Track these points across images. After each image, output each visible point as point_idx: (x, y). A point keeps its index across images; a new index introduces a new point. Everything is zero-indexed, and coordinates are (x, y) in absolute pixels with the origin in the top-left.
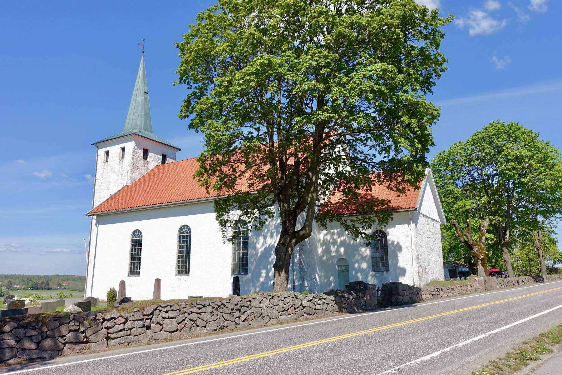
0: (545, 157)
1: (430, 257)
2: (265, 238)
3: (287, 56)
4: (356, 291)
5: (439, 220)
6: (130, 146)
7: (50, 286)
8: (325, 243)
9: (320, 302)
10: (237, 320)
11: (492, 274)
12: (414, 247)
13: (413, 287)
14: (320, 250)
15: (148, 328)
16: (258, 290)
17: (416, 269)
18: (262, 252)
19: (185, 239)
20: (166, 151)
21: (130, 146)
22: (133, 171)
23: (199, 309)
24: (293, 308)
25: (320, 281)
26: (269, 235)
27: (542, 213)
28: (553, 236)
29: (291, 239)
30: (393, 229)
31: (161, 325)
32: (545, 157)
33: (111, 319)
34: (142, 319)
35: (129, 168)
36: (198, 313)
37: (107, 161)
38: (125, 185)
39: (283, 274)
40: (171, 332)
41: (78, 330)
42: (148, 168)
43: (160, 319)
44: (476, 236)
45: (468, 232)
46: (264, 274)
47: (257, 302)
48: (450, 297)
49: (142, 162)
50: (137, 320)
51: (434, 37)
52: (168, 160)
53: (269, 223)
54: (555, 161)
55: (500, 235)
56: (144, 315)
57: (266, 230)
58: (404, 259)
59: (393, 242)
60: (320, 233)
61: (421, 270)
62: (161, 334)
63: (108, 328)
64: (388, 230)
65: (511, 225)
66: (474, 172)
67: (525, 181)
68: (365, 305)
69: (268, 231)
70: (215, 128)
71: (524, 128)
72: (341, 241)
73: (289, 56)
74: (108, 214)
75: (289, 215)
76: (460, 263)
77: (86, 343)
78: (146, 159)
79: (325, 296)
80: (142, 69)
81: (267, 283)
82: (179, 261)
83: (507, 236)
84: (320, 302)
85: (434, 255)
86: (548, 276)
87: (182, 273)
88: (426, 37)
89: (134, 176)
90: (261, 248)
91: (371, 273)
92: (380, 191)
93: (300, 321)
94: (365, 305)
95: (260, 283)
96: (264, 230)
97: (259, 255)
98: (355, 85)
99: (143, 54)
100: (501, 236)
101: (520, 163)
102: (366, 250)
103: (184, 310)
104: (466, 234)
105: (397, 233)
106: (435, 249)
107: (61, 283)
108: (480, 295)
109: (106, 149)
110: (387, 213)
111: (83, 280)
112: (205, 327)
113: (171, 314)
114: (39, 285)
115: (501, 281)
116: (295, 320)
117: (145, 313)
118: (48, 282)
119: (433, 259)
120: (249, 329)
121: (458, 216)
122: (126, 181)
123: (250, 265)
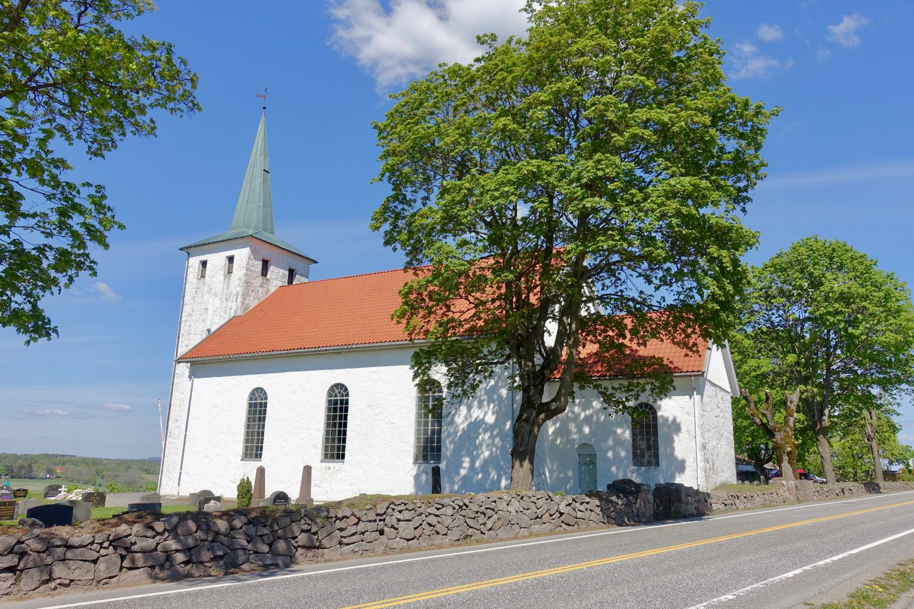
0: (888, 297)
1: (719, 446)
2: (469, 408)
3: (560, 161)
4: (626, 493)
5: (729, 390)
6: (242, 255)
7: (34, 473)
9: (582, 508)
10: (483, 529)
11: (805, 476)
12: (698, 432)
13: (698, 490)
15: (382, 532)
16: (456, 487)
17: (701, 464)
19: (338, 410)
20: (295, 263)
21: (242, 255)
22: (245, 295)
23: (438, 509)
24: (547, 514)
25: (550, 477)
27: (879, 382)
28: (895, 419)
29: (538, 414)
31: (397, 529)
32: (888, 297)
33: (344, 517)
34: (375, 521)
35: (240, 289)
36: (437, 516)
37: (203, 276)
38: (232, 315)
39: (526, 463)
40: (408, 540)
41: (309, 531)
42: (268, 291)
43: (394, 522)
44: (779, 417)
45: (767, 409)
47: (505, 504)
48: (502, 540)
49: (260, 279)
50: (370, 521)
51: (754, 137)
52: (298, 279)
54: (900, 303)
55: (814, 416)
56: (377, 515)
58: (683, 446)
59: (666, 420)
61: (708, 466)
62: (398, 542)
63: (341, 530)
65: (829, 400)
66: (773, 314)
67: (857, 332)
68: (638, 516)
70: (447, 253)
71: (854, 250)
72: (586, 417)
73: (562, 161)
74: (208, 360)
75: (534, 379)
76: (756, 461)
77: (318, 548)
78: (266, 275)
79: (587, 499)
80: (262, 134)
81: (473, 478)
82: (327, 439)
83: (826, 418)
84: (582, 508)
85: (724, 444)
86: (886, 483)
87: (251, 457)
88: (742, 136)
89: (247, 302)
90: (462, 423)
91: (632, 468)
92: (659, 348)
93: (558, 533)
94: (638, 516)
98: (655, 206)
99: (263, 111)
100: (816, 418)
101: (848, 304)
102: (624, 432)
103: (421, 510)
104: (765, 412)
105: (670, 407)
106: (726, 434)
107: (53, 468)
108: (791, 508)
109: (203, 258)
110: (664, 379)
111: (153, 467)
112: (446, 535)
113: (407, 515)
114: (15, 470)
115: (819, 489)
116: (551, 533)
117: (378, 512)
118: (30, 466)
119: (723, 450)
120: (498, 541)
121: (748, 383)
122: (234, 308)
123: (443, 450)
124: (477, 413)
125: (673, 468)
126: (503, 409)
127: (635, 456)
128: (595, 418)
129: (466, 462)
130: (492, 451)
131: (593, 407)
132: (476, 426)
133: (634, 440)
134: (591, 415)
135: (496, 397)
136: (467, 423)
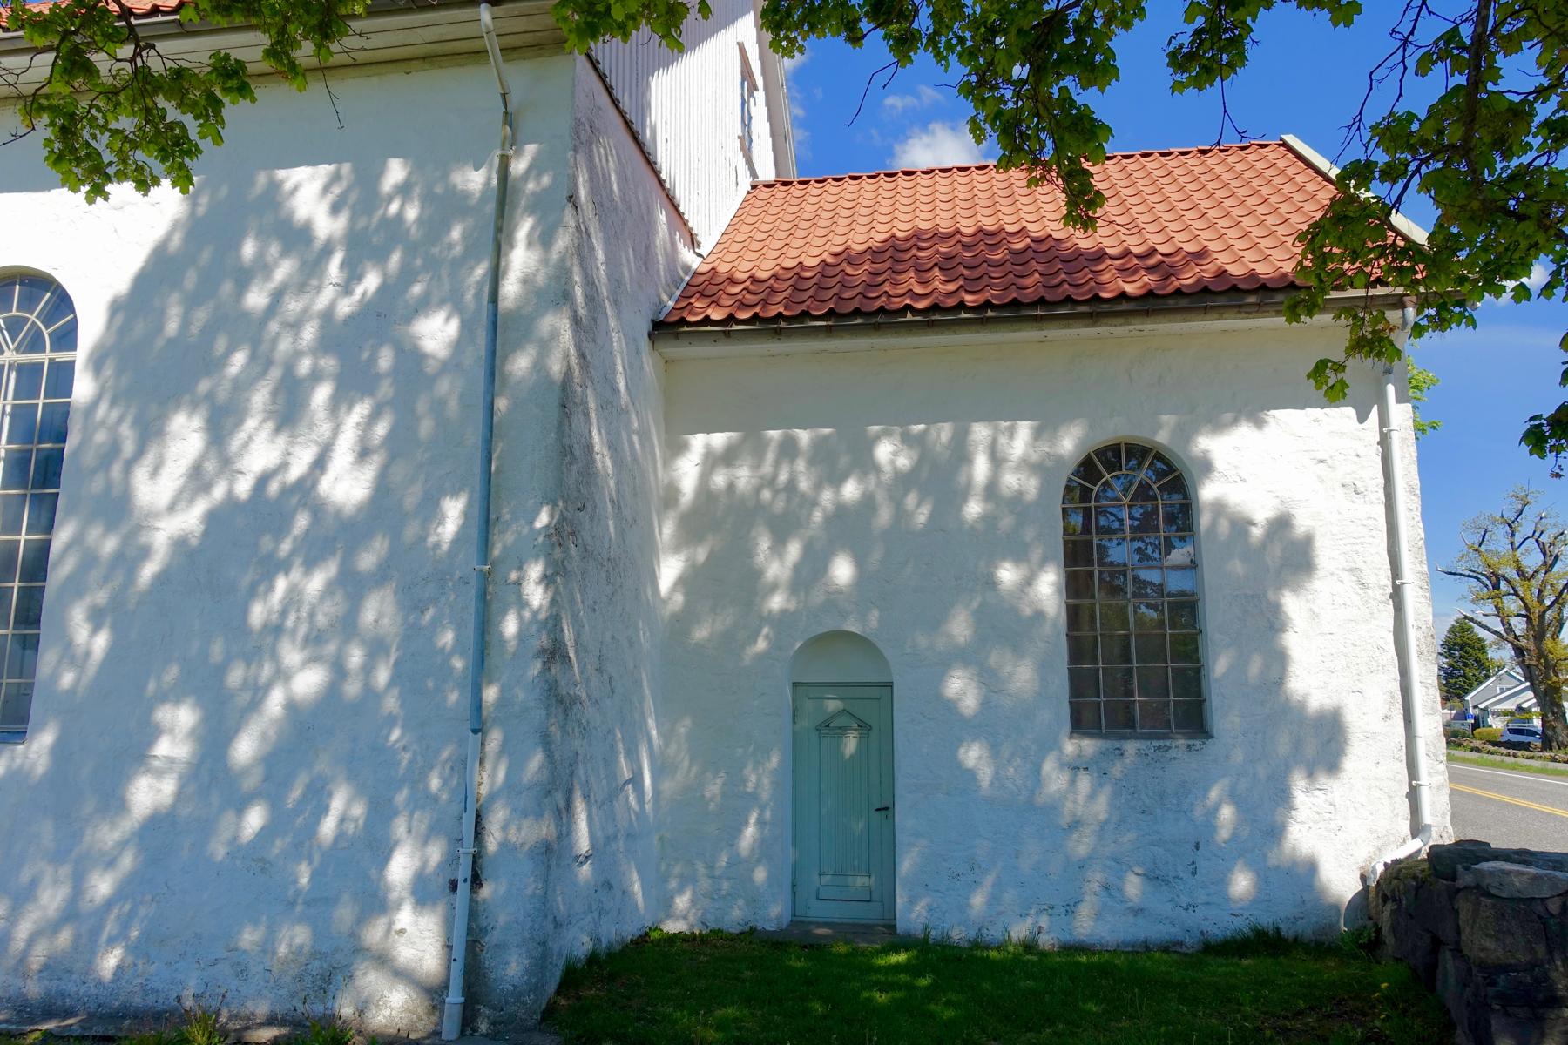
2: (221, 424)
8: (715, 518)
14: (669, 571)
18: (180, 544)
26: (260, 398)
30: (1244, 433)
46: (171, 748)
53: (278, 296)
57: (239, 359)
59: (1241, 525)
60: (677, 448)
64: (1207, 443)
69: (261, 362)
81: (206, 827)
90: (172, 508)
95: (128, 824)
96: (224, 361)
97: (148, 571)
102: (1029, 581)
124: (260, 451)
125: (1283, 746)
126: (426, 427)
127: (1080, 685)
128: (884, 516)
129: (177, 731)
130: (339, 670)
131: (876, 468)
132: (251, 532)
133: (1074, 614)
134: (867, 503)
135: (385, 360)
136: (200, 507)
